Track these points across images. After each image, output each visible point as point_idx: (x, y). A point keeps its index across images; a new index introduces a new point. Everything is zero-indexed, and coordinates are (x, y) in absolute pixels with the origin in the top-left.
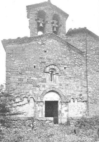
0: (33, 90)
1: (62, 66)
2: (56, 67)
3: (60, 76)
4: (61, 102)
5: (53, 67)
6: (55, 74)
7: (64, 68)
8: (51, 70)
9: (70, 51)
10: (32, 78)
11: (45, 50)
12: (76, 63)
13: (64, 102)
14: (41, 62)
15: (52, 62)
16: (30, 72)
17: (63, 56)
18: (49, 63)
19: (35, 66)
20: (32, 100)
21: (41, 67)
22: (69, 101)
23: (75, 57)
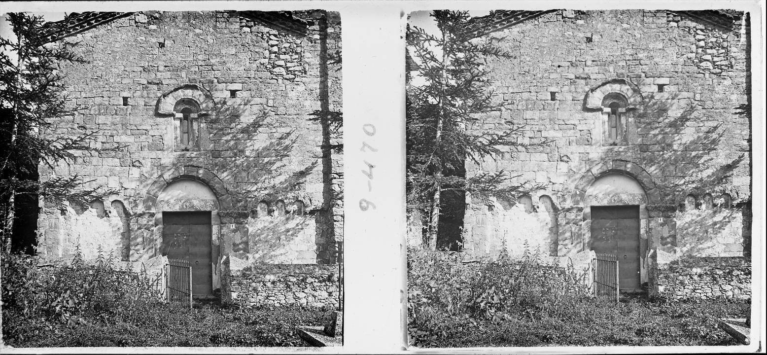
0: (120, 178)
1: (220, 86)
2: (197, 93)
3: (213, 122)
4: (646, 208)
5: (189, 93)
6: (196, 119)
7: (656, 88)
8: (609, 102)
9: (254, 29)
10: (116, 139)
11: (589, 35)
12: (277, 70)
13: (228, 215)
14: (573, 77)
15: (184, 76)
16: (110, 118)
17: (651, 46)
18: (600, 76)
19: (125, 99)
20: (543, 207)
21: (575, 95)
22: (677, 204)
23: (702, 43)
